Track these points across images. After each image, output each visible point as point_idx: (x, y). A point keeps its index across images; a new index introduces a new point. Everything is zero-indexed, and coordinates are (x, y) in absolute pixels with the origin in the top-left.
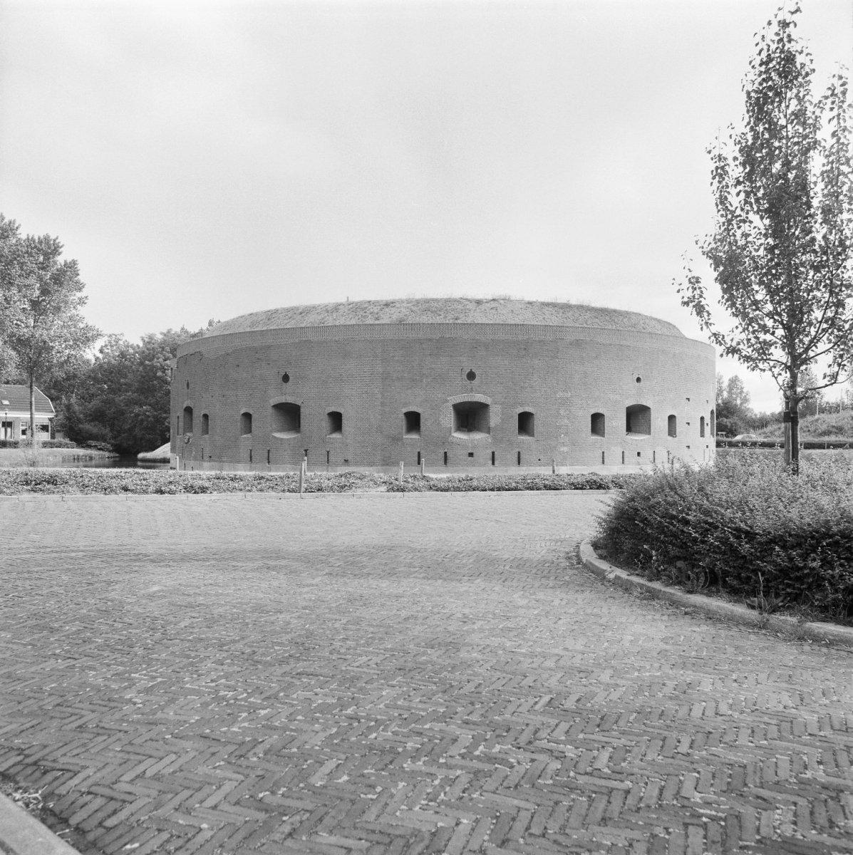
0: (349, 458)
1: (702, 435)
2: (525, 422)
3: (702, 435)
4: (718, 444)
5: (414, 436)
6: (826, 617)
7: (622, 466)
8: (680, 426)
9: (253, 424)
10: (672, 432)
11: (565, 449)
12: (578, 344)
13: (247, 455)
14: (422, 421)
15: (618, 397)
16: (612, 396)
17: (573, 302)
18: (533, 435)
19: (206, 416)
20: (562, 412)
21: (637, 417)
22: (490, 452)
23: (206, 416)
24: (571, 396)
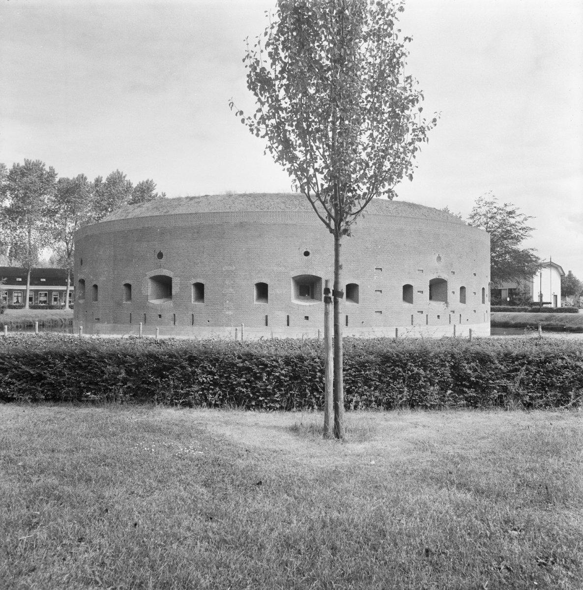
0: (100, 317)
1: (483, 302)
2: (200, 289)
3: (483, 302)
4: (492, 310)
5: (129, 302)
6: (108, 398)
7: (287, 327)
8: (469, 293)
9: (132, 290)
10: (463, 300)
11: (230, 313)
12: (242, 225)
13: (190, 321)
14: (269, 289)
15: (282, 269)
16: (275, 268)
17: (248, 193)
18: (357, 302)
19: (128, 286)
20: (227, 282)
21: (437, 288)
22: (172, 314)
23: (96, 286)
24: (236, 269)
